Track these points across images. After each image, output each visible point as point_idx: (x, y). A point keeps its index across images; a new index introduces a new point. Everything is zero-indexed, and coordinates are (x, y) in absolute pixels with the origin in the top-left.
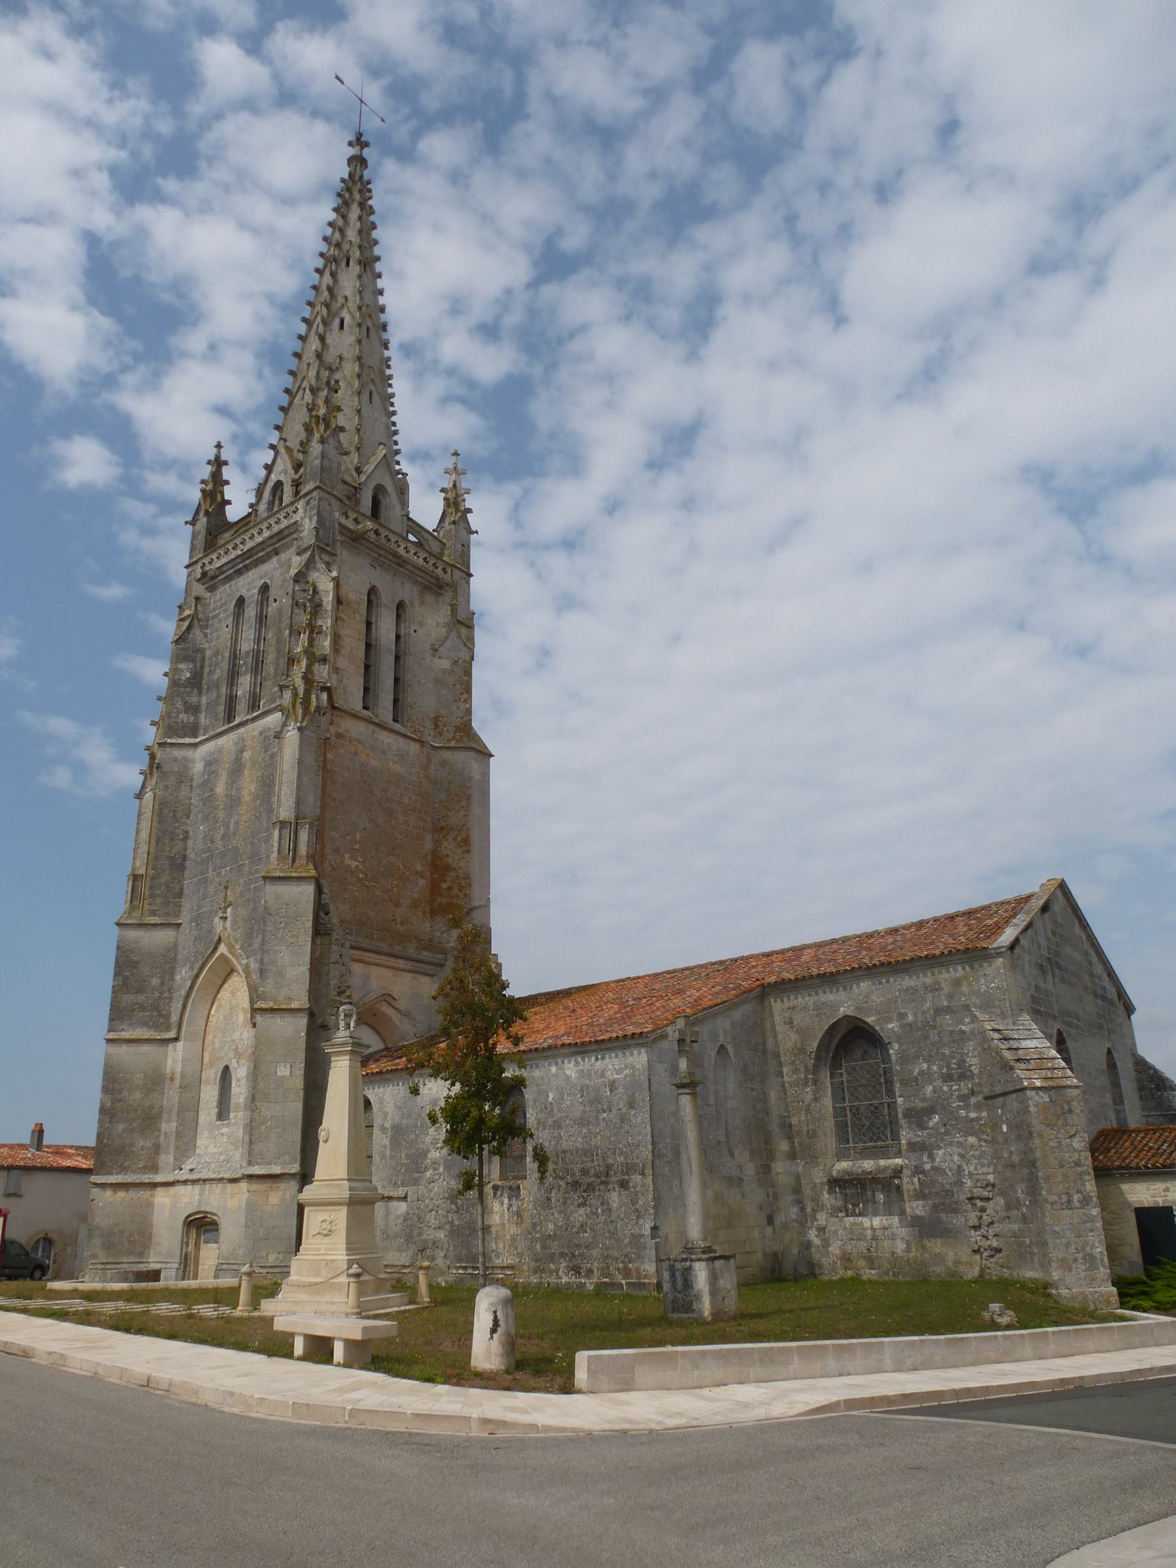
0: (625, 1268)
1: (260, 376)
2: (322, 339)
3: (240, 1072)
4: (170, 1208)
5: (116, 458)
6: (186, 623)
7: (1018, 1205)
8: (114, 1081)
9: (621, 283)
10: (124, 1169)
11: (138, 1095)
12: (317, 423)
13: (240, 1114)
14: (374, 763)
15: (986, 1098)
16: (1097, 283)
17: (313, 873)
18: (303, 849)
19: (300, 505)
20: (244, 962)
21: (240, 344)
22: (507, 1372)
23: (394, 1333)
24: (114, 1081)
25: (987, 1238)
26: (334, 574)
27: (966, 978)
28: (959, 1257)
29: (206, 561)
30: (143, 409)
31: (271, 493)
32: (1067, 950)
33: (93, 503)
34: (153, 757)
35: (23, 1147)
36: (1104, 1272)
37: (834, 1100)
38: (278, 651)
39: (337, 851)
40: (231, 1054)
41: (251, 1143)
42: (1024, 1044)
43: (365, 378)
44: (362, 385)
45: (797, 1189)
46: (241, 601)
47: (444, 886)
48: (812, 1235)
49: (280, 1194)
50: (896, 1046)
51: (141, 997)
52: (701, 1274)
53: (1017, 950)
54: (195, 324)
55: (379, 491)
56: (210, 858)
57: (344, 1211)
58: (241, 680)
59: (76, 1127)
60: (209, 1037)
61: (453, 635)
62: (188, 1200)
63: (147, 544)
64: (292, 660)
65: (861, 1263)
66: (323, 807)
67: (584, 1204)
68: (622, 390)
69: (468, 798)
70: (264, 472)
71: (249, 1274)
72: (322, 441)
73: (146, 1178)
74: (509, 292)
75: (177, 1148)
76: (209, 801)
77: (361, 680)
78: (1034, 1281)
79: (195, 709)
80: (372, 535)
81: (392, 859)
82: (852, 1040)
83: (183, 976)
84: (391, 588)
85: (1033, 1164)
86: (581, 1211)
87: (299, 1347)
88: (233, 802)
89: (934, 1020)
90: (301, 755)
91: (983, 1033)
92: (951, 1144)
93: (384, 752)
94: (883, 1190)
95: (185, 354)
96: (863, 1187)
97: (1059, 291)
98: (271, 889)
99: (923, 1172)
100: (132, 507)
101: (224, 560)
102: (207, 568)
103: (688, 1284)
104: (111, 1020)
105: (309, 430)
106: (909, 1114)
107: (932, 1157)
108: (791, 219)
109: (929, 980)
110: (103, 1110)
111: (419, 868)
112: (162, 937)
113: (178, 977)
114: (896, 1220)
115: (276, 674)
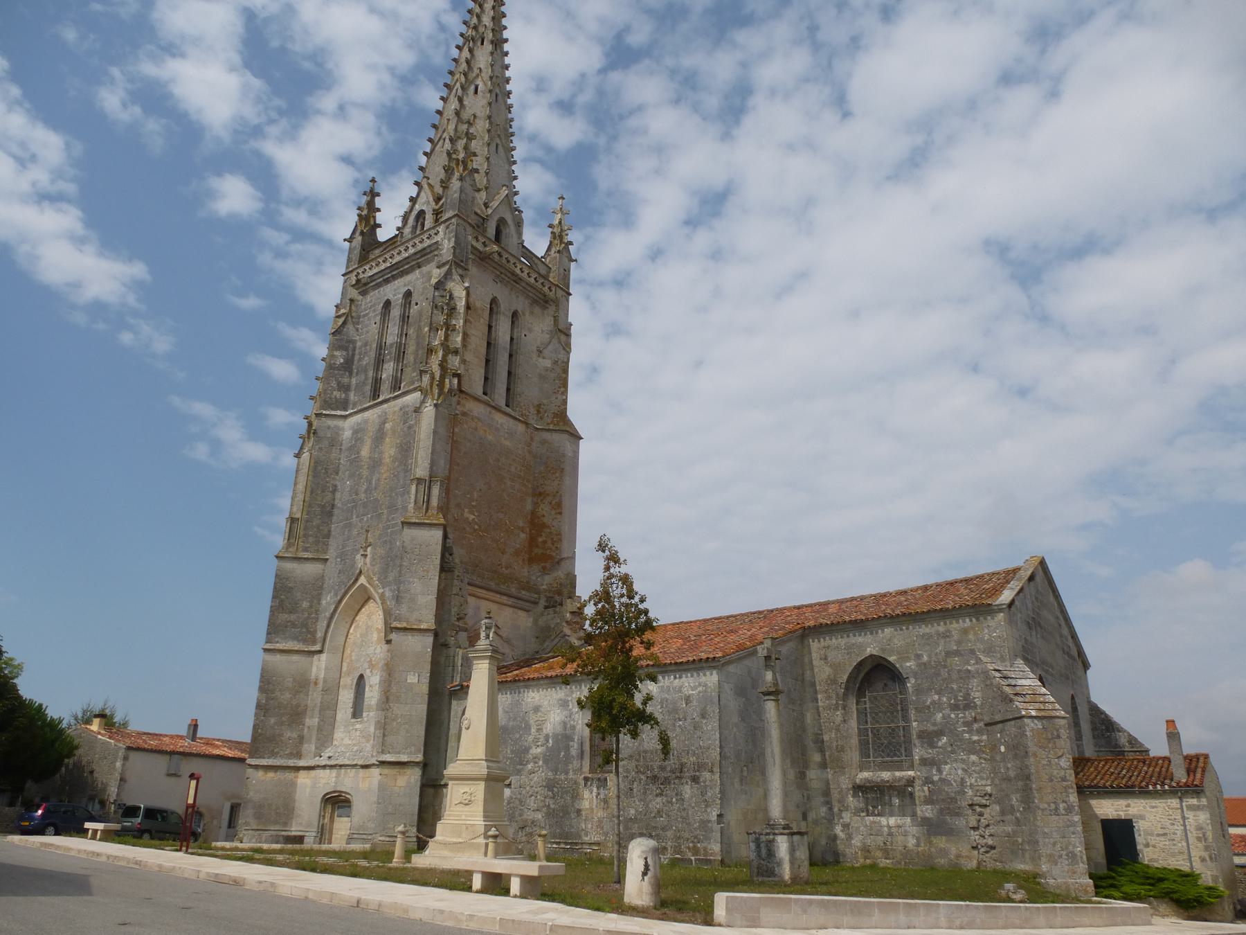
0: (695, 847)
1: (379, 133)
2: (460, 100)
3: (374, 681)
4: (310, 788)
5: (259, 194)
6: (342, 320)
7: (1012, 810)
8: (269, 683)
9: (673, 73)
10: (273, 755)
11: (288, 695)
12: (458, 164)
13: (372, 714)
14: (490, 437)
15: (986, 725)
16: (1054, 94)
17: (442, 521)
18: (434, 502)
19: (441, 229)
20: (381, 591)
21: (363, 106)
22: (655, 908)
23: (562, 872)
24: (269, 683)
25: (983, 837)
26: (467, 285)
27: (973, 628)
28: (960, 851)
29: (360, 271)
30: (283, 155)
31: (415, 219)
32: (1045, 613)
33: (239, 229)
34: (310, 424)
35: (181, 737)
36: (1083, 867)
37: (859, 723)
38: (418, 344)
39: (458, 505)
40: (366, 665)
41: (384, 735)
42: (1020, 682)
43: (493, 132)
44: (491, 138)
45: (827, 793)
46: (388, 304)
47: (540, 540)
48: (838, 830)
49: (406, 778)
50: (913, 681)
51: (294, 616)
52: (782, 846)
53: (1013, 608)
54: (329, 88)
55: (501, 222)
56: (355, 507)
57: (482, 785)
58: (386, 366)
59: (231, 721)
60: (348, 651)
61: (555, 341)
62: (326, 781)
63: (279, 265)
64: (430, 351)
65: (879, 854)
66: (450, 470)
67: (661, 795)
68: (668, 159)
69: (562, 470)
70: (408, 204)
71: (403, 833)
72: (461, 179)
73: (291, 763)
74: (583, 75)
75: (318, 739)
76: (355, 461)
77: (483, 371)
78: (1025, 872)
79: (346, 388)
80: (496, 256)
81: (501, 516)
82: (875, 675)
83: (328, 600)
84: (510, 300)
85: (1028, 778)
86: (659, 799)
87: (477, 882)
88: (375, 464)
89: (945, 661)
90: (436, 425)
91: (986, 672)
92: (956, 760)
93: (497, 429)
94: (898, 796)
95: (319, 112)
96: (882, 792)
97: (1022, 99)
98: (409, 533)
99: (932, 782)
100: (268, 234)
101: (375, 271)
102: (361, 276)
103: (771, 854)
104: (269, 633)
105: (448, 171)
106: (922, 735)
107: (940, 771)
108: (813, 29)
109: (941, 629)
110: (259, 706)
111: (521, 524)
112: (312, 569)
113: (324, 602)
114: (908, 820)
115: (415, 362)
